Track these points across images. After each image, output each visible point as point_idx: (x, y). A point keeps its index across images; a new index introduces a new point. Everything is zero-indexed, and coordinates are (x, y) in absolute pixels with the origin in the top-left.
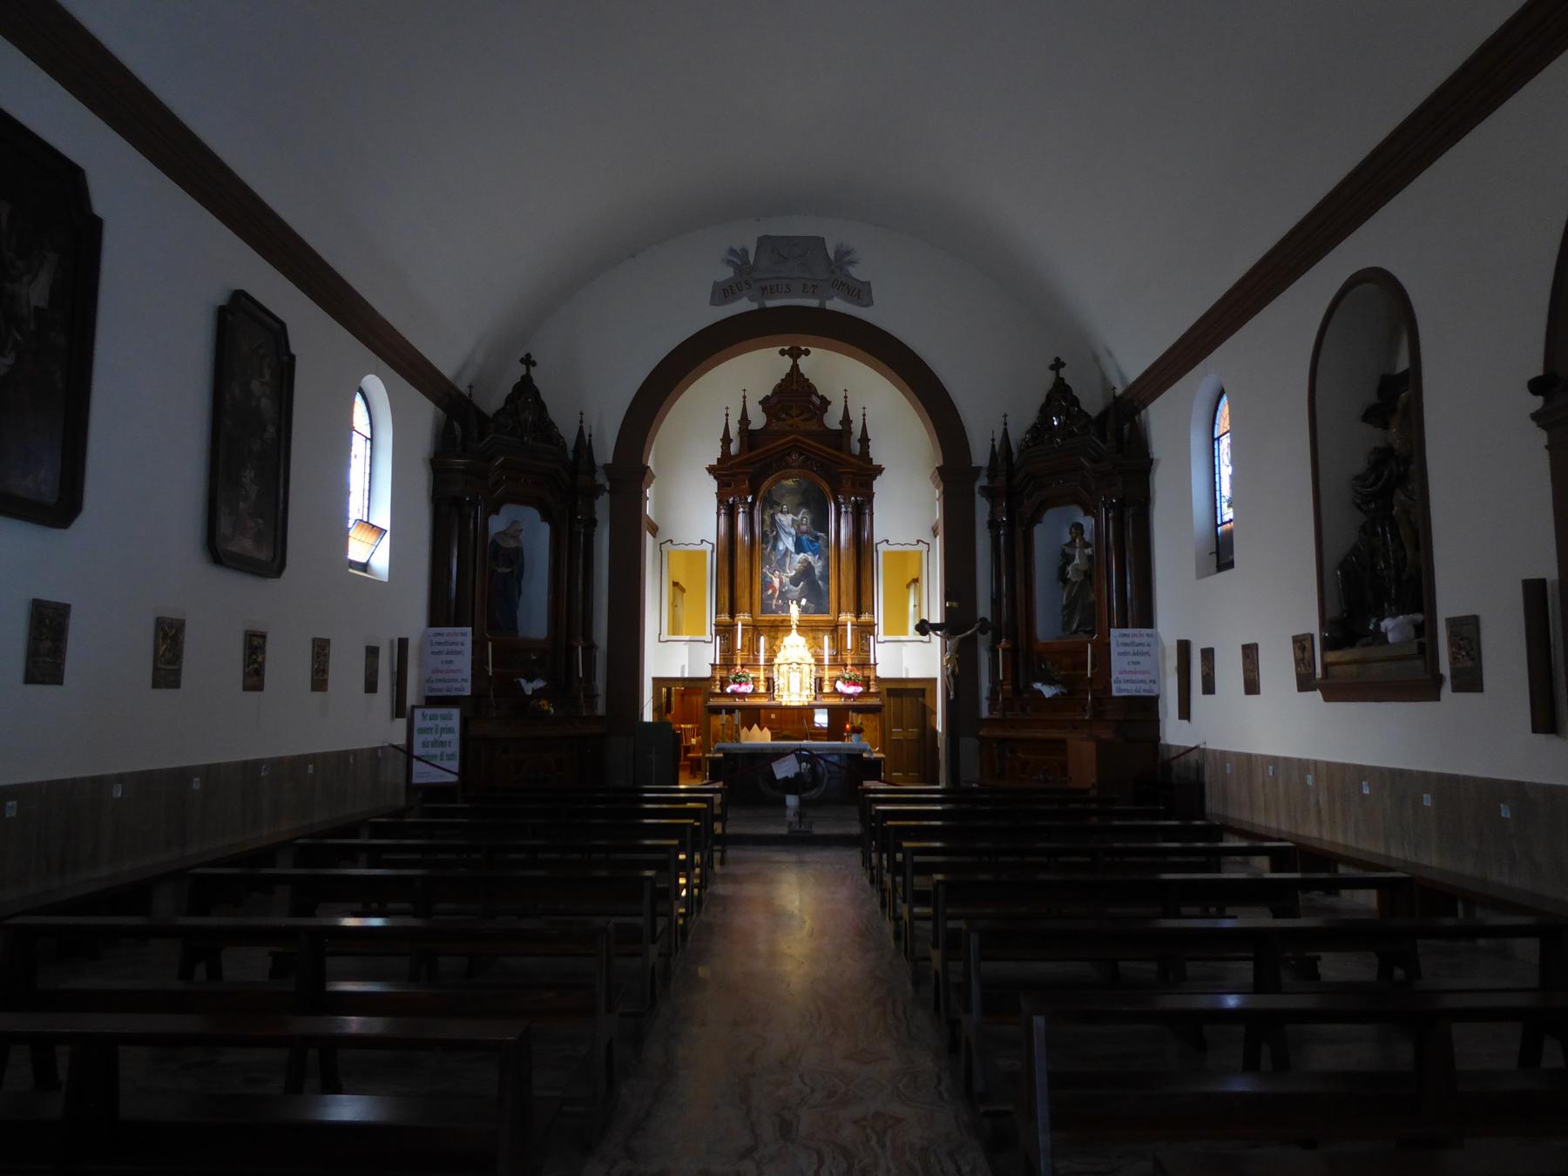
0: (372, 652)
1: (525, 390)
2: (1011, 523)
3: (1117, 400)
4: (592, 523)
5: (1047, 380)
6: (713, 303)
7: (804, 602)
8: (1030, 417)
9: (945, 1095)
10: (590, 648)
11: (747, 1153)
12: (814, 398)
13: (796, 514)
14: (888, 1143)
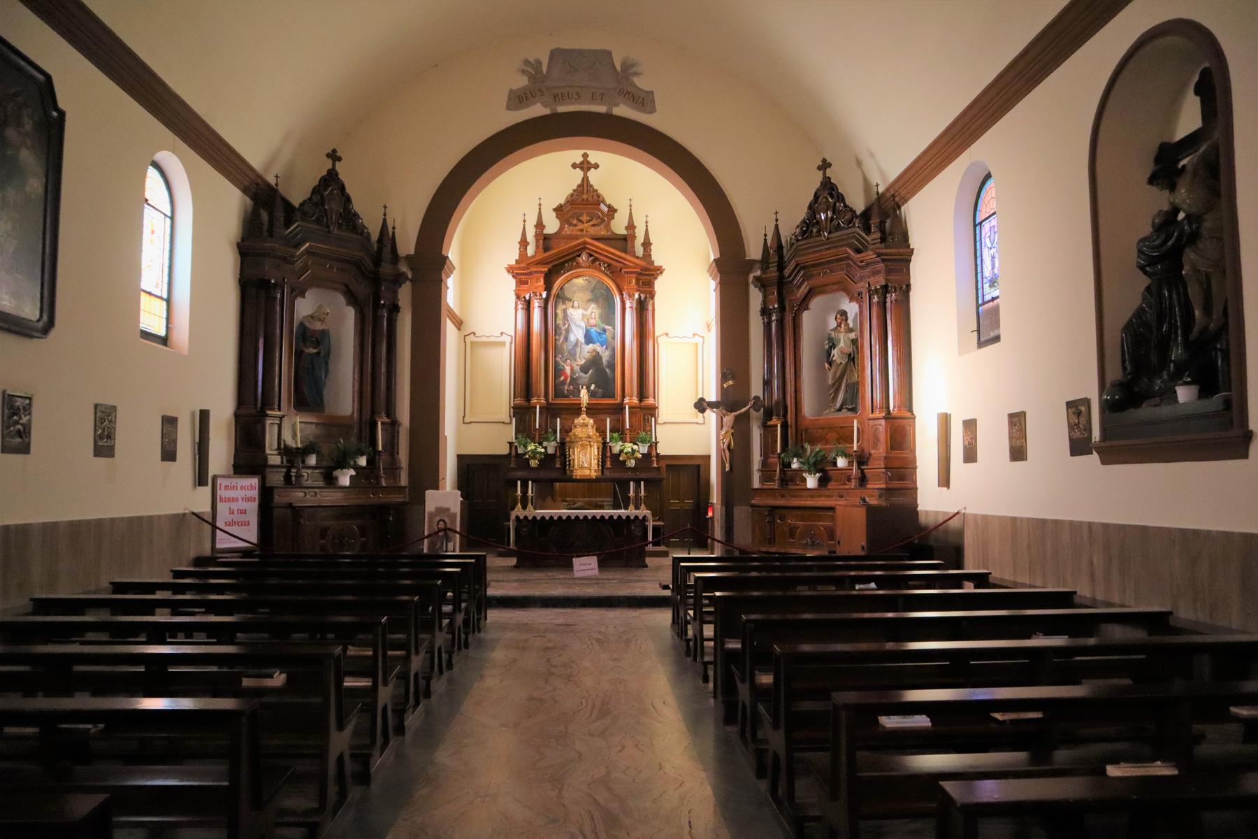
0: (170, 423)
1: (331, 180)
2: (782, 309)
3: (880, 197)
4: (395, 308)
5: (817, 178)
6: (509, 108)
7: (593, 387)
8: (800, 213)
10: (393, 425)
12: (603, 207)
13: (586, 309)
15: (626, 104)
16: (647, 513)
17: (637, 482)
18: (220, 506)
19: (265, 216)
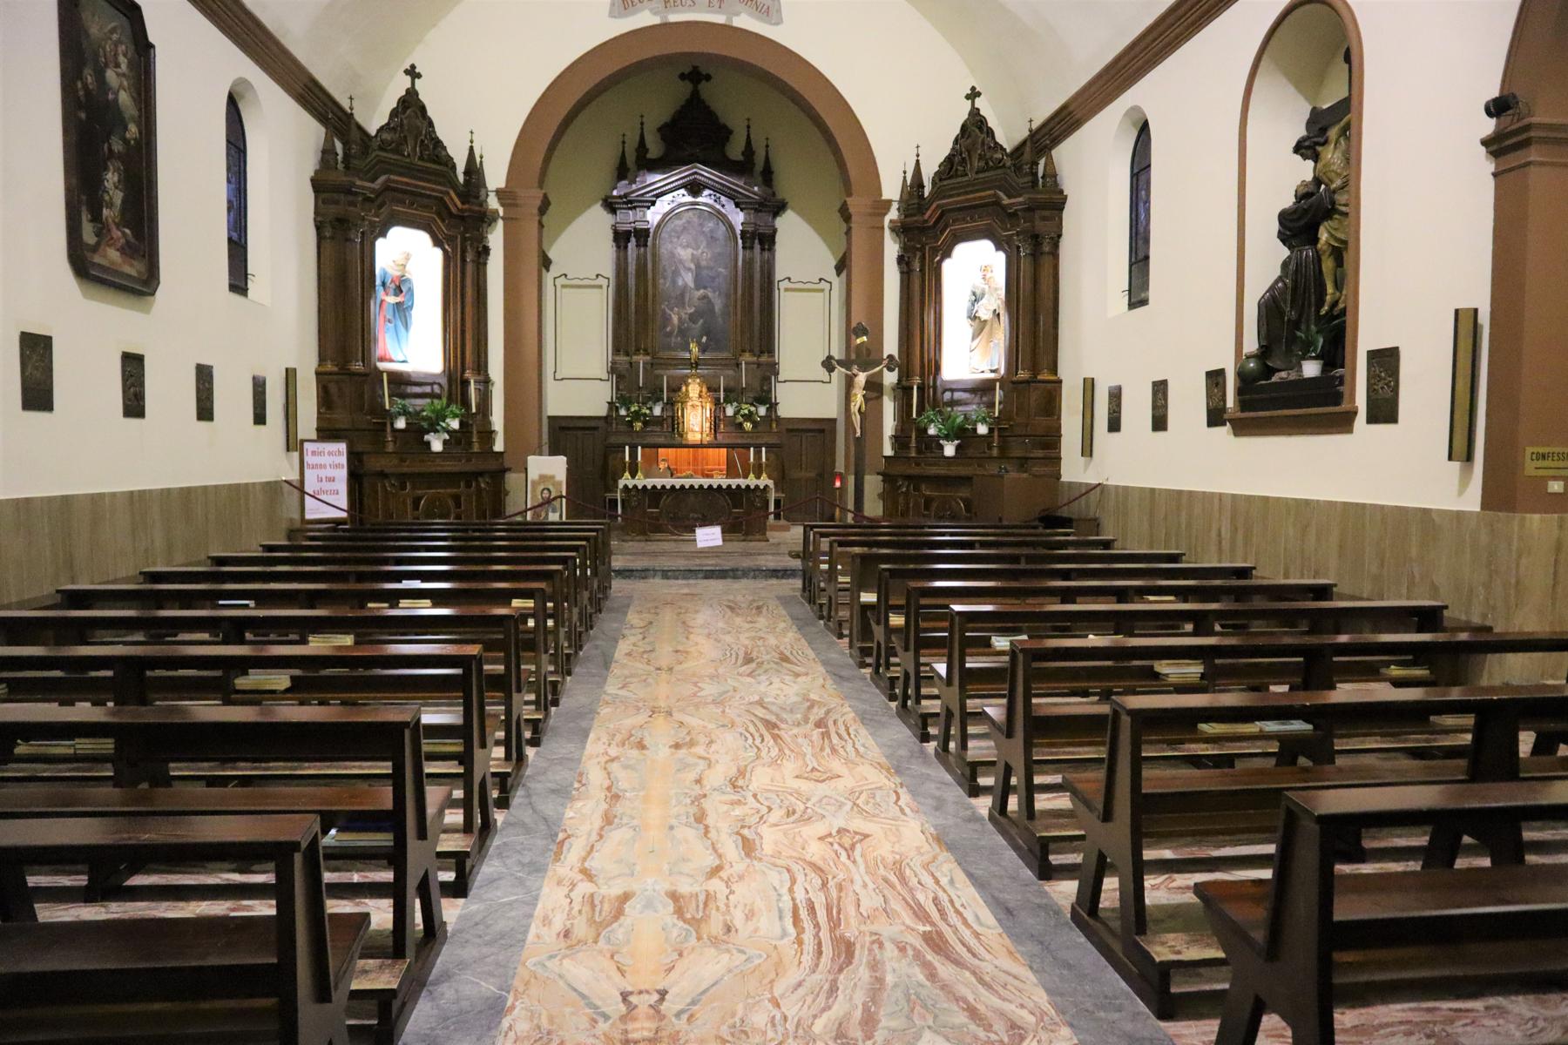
0: (259, 387)
5: (962, 112)
6: (612, 15)
9: (907, 810)
10: (487, 382)
11: (715, 871)
14: (859, 860)
15: (750, 15)
16: (771, 483)
17: (758, 448)
18: (307, 472)
19: (339, 146)
